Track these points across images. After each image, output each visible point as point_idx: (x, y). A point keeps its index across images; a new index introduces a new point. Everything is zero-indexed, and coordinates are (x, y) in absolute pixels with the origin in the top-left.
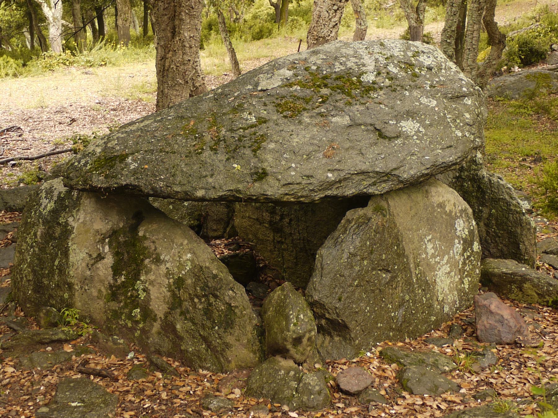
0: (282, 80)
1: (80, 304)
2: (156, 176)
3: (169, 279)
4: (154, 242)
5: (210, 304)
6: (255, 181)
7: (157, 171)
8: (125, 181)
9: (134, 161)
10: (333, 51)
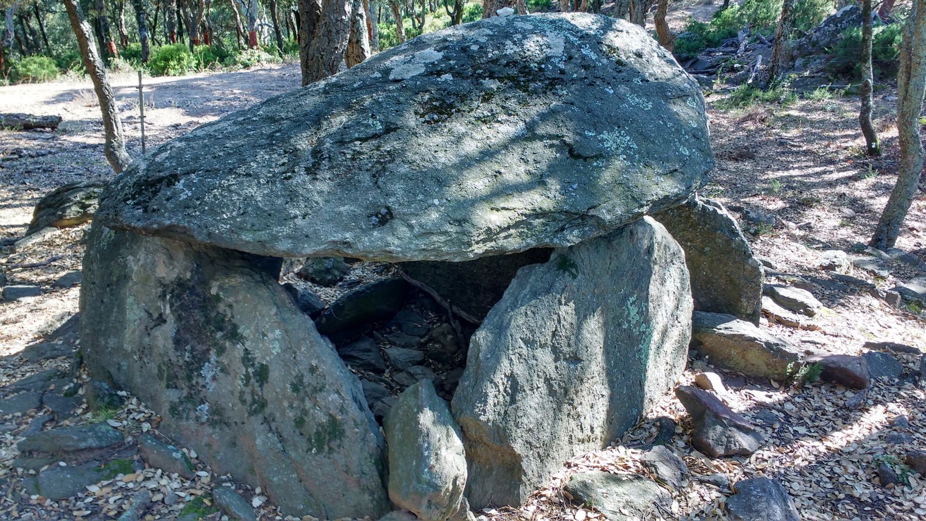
0: (426, 65)
1: (139, 380)
2: (217, 214)
3: (247, 367)
4: (230, 306)
5: (305, 412)
6: (374, 226)
7: (218, 206)
8: (170, 218)
9: (188, 186)
10: (504, 24)
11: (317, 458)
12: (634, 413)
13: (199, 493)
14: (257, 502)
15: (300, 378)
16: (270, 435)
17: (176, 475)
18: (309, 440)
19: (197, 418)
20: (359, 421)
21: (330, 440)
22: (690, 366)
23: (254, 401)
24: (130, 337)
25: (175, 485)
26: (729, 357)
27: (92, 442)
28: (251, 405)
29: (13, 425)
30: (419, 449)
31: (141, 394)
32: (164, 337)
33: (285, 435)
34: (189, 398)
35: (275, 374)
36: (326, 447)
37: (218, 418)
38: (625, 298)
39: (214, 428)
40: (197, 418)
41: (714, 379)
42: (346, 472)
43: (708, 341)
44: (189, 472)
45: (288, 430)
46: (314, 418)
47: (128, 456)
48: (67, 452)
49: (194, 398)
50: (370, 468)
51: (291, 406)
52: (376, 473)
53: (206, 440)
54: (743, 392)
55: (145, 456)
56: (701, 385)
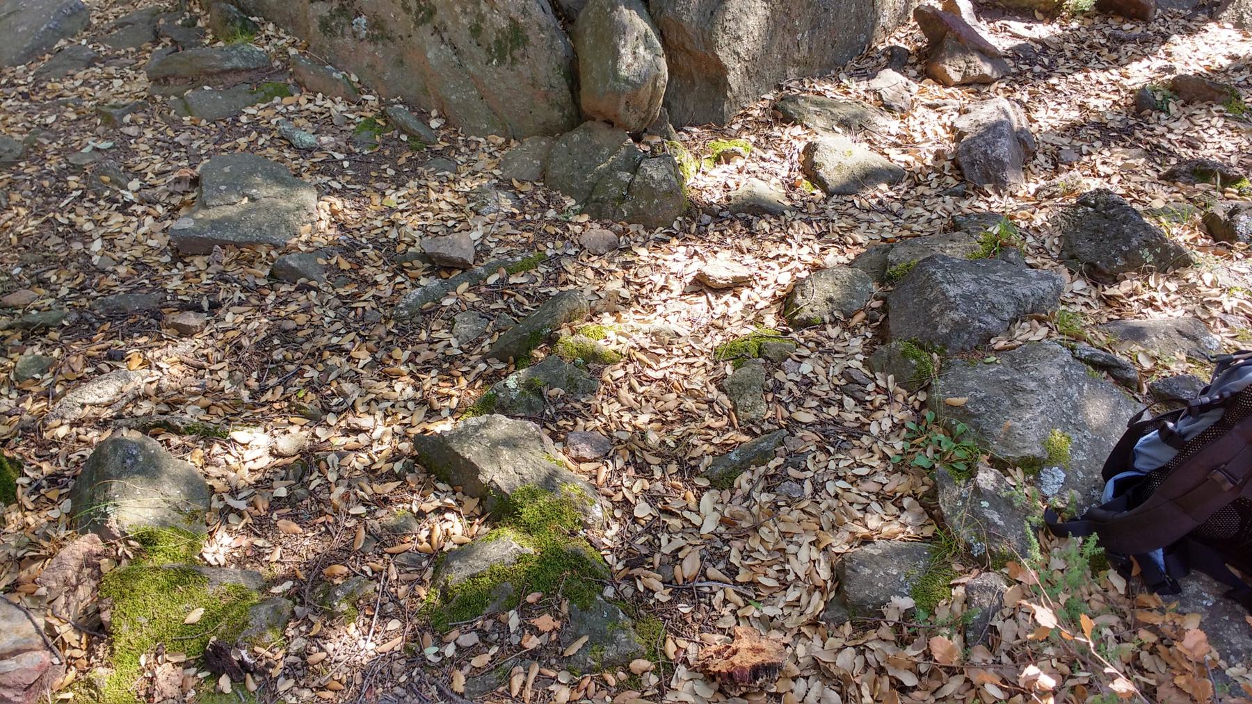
5: (481, 18)
11: (499, 70)
12: (862, 40)
13: (370, 115)
14: (434, 124)
16: (443, 47)
17: (339, 99)
18: (489, 50)
19: (354, 34)
20: (544, 26)
21: (512, 49)
23: (420, 9)
25: (341, 107)
27: (236, 62)
28: (417, 14)
29: (130, 60)
31: (277, 18)
33: (460, 46)
36: (509, 58)
39: (376, 44)
40: (354, 34)
42: (533, 85)
44: (353, 97)
45: (463, 40)
46: (492, 25)
47: (280, 80)
48: (210, 75)
50: (559, 81)
51: (464, 11)
52: (565, 87)
53: (367, 60)
54: (998, 24)
55: (301, 79)
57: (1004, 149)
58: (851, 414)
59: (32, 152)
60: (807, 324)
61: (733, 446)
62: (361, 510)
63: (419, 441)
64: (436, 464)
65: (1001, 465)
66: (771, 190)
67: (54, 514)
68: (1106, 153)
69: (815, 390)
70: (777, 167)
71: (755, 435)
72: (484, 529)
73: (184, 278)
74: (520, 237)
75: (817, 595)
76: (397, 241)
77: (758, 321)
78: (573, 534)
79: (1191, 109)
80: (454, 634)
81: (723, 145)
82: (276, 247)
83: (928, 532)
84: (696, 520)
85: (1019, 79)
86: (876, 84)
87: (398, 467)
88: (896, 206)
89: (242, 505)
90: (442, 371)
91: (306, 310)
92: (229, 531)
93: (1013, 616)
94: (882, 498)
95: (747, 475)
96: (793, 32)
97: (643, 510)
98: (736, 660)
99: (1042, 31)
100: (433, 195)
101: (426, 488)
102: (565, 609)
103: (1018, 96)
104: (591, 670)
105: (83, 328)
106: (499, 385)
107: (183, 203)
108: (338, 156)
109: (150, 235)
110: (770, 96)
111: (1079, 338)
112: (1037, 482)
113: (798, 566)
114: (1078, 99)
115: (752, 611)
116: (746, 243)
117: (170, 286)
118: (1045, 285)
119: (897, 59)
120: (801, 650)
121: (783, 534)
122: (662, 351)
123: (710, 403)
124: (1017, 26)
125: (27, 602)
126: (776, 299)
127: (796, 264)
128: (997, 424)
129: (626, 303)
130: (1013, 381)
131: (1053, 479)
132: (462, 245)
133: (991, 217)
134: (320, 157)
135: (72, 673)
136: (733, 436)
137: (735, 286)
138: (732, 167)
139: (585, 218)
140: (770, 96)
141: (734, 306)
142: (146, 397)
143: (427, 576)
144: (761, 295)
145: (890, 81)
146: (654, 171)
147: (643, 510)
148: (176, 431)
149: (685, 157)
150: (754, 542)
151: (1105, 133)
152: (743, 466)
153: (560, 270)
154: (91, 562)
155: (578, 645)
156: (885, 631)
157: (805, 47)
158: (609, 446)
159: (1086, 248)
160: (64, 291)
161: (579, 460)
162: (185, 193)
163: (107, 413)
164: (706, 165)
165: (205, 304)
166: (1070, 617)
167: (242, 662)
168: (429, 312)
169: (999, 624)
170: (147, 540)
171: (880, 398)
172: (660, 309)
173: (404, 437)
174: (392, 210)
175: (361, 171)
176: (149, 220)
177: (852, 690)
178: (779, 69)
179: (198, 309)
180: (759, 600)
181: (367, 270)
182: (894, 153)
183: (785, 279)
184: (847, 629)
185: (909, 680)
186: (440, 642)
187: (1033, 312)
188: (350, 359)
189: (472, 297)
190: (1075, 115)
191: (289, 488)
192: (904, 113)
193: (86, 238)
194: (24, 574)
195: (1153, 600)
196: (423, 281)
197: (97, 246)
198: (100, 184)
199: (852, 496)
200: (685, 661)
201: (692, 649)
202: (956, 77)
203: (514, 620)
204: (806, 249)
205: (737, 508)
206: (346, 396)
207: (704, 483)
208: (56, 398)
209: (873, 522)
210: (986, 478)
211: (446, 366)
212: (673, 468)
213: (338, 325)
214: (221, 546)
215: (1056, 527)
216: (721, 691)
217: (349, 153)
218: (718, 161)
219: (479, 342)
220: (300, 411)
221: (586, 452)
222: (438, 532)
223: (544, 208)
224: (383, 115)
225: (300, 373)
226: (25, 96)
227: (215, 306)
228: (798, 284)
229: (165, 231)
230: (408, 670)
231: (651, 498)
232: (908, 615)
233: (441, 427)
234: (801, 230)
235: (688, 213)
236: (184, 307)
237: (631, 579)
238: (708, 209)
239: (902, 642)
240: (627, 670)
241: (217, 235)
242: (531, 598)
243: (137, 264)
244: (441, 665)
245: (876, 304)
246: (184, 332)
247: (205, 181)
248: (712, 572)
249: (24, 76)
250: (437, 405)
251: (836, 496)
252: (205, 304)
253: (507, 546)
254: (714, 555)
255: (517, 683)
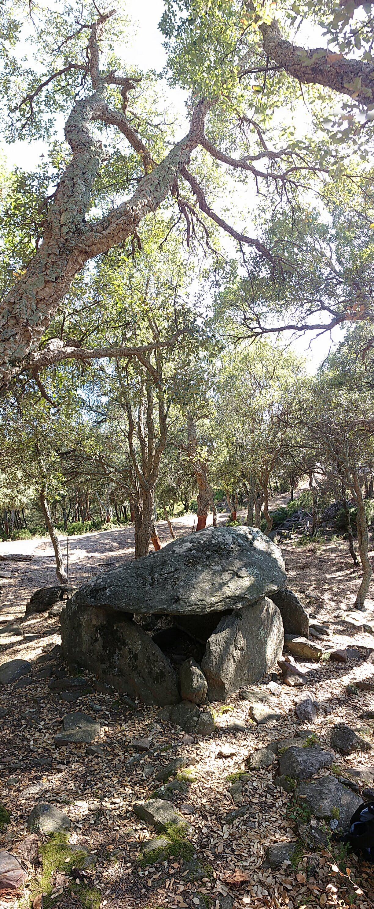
14: (137, 702)
15: (149, 657)
22: (283, 655)
24: (85, 647)
26: (297, 652)
30: (191, 674)
32: (98, 646)
34: (110, 667)
35: (140, 656)
37: (121, 673)
38: (259, 628)
41: (292, 659)
43: (290, 645)
49: (112, 666)
56: (288, 661)
57: (310, 709)
58: (270, 800)
59: (10, 713)
60: (254, 769)
61: (233, 810)
62: (118, 828)
63: (135, 806)
64: (140, 815)
65: (318, 819)
66: (240, 723)
67: (22, 827)
68: (341, 708)
69: (258, 791)
70: (241, 715)
71: (239, 807)
72: (156, 835)
73: (59, 753)
74: (163, 739)
75: (260, 859)
76: (125, 741)
77: (239, 768)
78: (184, 837)
79: (364, 693)
80: (148, 868)
81: (225, 708)
82: (87, 743)
83: (295, 840)
84: (222, 834)
85: (311, 683)
86: (268, 686)
87: (128, 815)
88: (279, 728)
89: (81, 826)
90: (140, 785)
91: (98, 764)
92: (77, 834)
93: (322, 868)
94: (280, 828)
95: (237, 820)
96: (243, 671)
97: (205, 830)
98: (235, 879)
99: (316, 666)
100: (137, 725)
101: (137, 822)
102: (182, 861)
103: (312, 689)
104: (190, 881)
105: (28, 769)
106: (158, 789)
107: (58, 729)
108: (107, 713)
109: (48, 739)
110: (238, 691)
111: (339, 775)
112: (329, 824)
113: (254, 849)
114: (330, 690)
115: (240, 863)
116: (234, 740)
117: (55, 756)
118: (328, 757)
119: (274, 678)
120: (255, 877)
121: (249, 839)
122: (209, 778)
123: (225, 796)
124: (308, 665)
125: (15, 855)
126: (244, 760)
127: (250, 748)
128: (316, 804)
129: (197, 762)
130: (321, 790)
131: (335, 824)
132: (145, 742)
133: (308, 732)
134: (102, 713)
135: (31, 876)
136: (232, 807)
137: (232, 755)
138: (228, 715)
139: (183, 733)
140: (238, 691)
141: (230, 762)
142: (49, 791)
143: (139, 850)
144: (238, 759)
145: (273, 685)
146: (204, 717)
147: (205, 830)
148: (59, 802)
149: (213, 712)
150: (240, 842)
151: (341, 702)
152: (236, 817)
153: (176, 751)
154: (34, 842)
155: (186, 872)
156: (282, 871)
157: (246, 675)
158: (193, 810)
159: (339, 743)
160: (21, 758)
161: (184, 814)
162: (58, 726)
163: (37, 796)
164: (221, 714)
165: (65, 762)
166: (342, 868)
167: (83, 875)
168: (136, 765)
169: (318, 870)
170: (51, 835)
171: (278, 795)
172: (208, 764)
173: (130, 806)
174: (124, 731)
175: (114, 719)
176: (47, 734)
177: (271, 890)
178: (240, 682)
179: (63, 764)
180: (242, 860)
181: (116, 751)
182: (276, 709)
183: (247, 754)
184: (270, 870)
185: (290, 887)
186: (144, 870)
187: (325, 766)
188: (111, 780)
189: (149, 760)
190: (330, 696)
191: (95, 821)
192: (279, 696)
193: (28, 740)
194: (14, 846)
195: (367, 864)
196: (134, 755)
197: (32, 743)
198: (32, 722)
199: (271, 828)
200: (219, 879)
201: (221, 875)
202: (293, 684)
203: (166, 864)
204: (252, 743)
205: (234, 830)
206: (111, 792)
207: (224, 822)
208: (21, 791)
209: (277, 836)
210: (313, 823)
211: (142, 783)
212: (214, 817)
213: (107, 769)
214: (74, 839)
215: (336, 838)
216: (230, 889)
217: (111, 711)
218: (224, 713)
219: (152, 775)
220: (97, 796)
221: (186, 811)
222: (141, 836)
223: (171, 729)
224: (121, 699)
225: (96, 784)
226: (10, 694)
227: (68, 762)
228: (251, 755)
229: (53, 738)
230: (134, 879)
231: (207, 827)
232: (289, 866)
233: (140, 802)
234: (251, 736)
235: (215, 731)
236: (59, 763)
237: (202, 852)
238: (222, 729)
239: (287, 875)
240: (201, 881)
241: (69, 739)
242: (171, 858)
243: (44, 748)
244: (144, 877)
245: (276, 762)
246: (59, 771)
247: (65, 722)
248: (227, 851)
249: (10, 687)
250: (139, 796)
251: (266, 827)
252: (65, 762)
253: (162, 841)
254: (228, 845)
255: (167, 884)
